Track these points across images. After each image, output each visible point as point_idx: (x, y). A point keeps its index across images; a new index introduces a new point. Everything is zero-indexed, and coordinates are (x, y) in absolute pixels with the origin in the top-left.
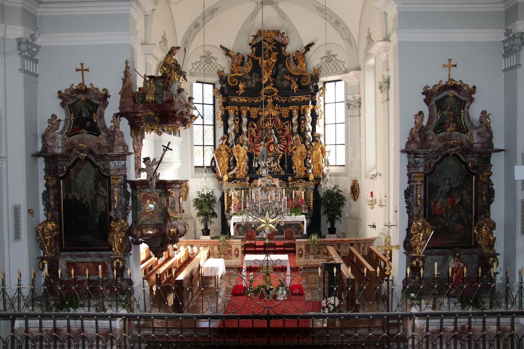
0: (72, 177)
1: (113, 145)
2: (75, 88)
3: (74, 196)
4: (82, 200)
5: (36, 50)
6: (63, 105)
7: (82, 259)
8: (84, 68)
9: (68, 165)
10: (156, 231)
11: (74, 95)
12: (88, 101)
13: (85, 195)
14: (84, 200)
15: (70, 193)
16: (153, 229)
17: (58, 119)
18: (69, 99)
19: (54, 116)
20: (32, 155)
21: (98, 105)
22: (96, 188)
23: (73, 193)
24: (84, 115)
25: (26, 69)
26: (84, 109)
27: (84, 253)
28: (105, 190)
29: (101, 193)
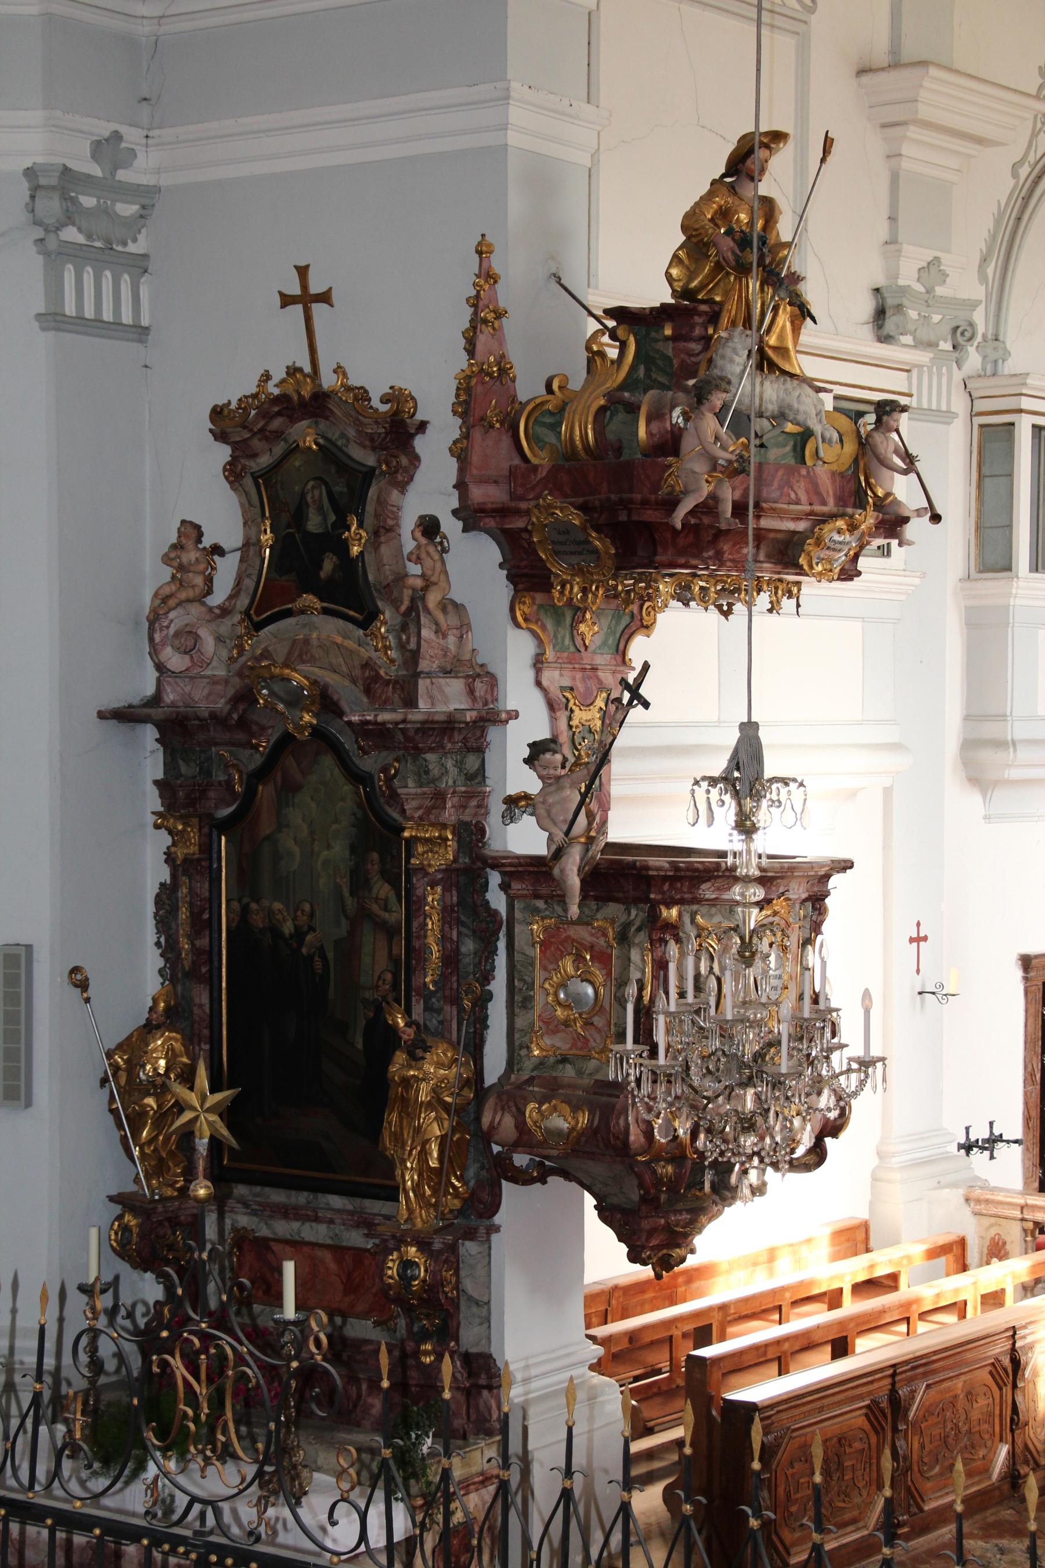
0: (266, 827)
1: (416, 675)
2: (276, 391)
3: (270, 912)
4: (299, 935)
5: (134, 208)
6: (233, 473)
7: (296, 1225)
8: (315, 288)
9: (252, 767)
10: (583, 1119)
11: (277, 423)
12: (330, 454)
13: (312, 915)
14: (309, 938)
15: (257, 901)
16: (575, 1109)
17: (207, 542)
18: (257, 444)
19: (192, 531)
20: (102, 715)
21: (369, 475)
22: (359, 882)
23: (265, 903)
24: (314, 523)
25: (70, 309)
26: (316, 494)
27: (301, 1198)
28: (392, 895)
29: (375, 908)
